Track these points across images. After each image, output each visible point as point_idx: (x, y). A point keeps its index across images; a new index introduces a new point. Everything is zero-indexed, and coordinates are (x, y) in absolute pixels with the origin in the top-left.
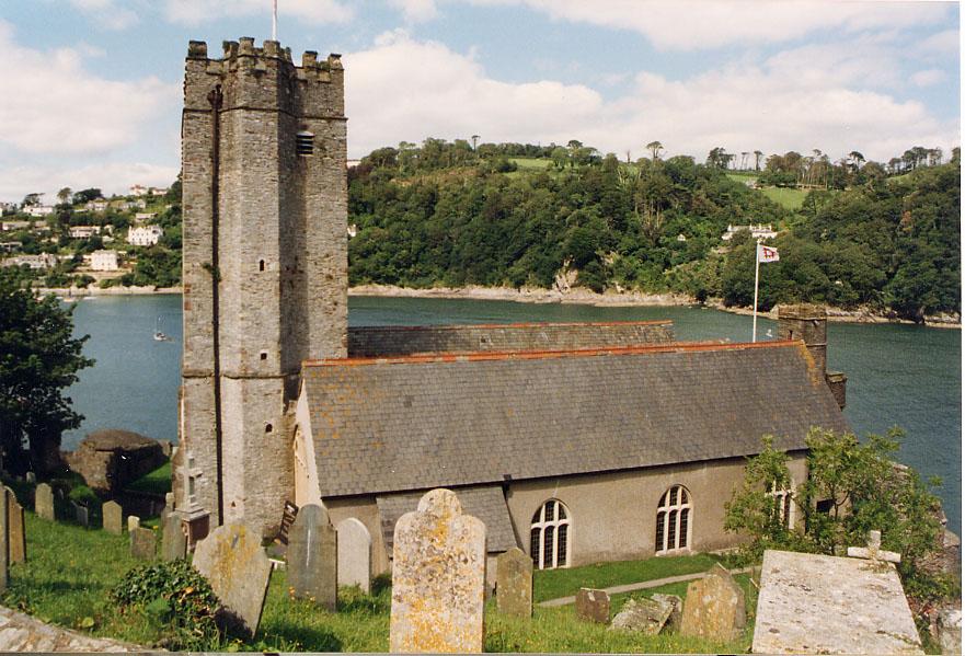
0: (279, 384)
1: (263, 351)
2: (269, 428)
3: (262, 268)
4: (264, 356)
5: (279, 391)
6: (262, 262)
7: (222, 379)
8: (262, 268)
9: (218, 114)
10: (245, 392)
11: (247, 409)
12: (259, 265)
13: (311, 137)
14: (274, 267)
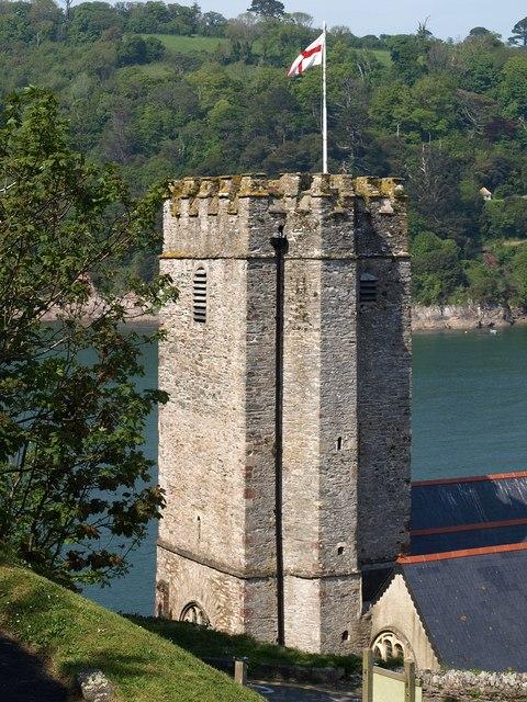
0: (358, 583)
1: (339, 545)
2: (345, 635)
3: (339, 448)
4: (341, 550)
5: (356, 591)
6: (339, 440)
7: (287, 580)
8: (339, 448)
9: (279, 261)
10: (323, 594)
11: (324, 614)
12: (336, 443)
13: (373, 282)
14: (350, 444)
